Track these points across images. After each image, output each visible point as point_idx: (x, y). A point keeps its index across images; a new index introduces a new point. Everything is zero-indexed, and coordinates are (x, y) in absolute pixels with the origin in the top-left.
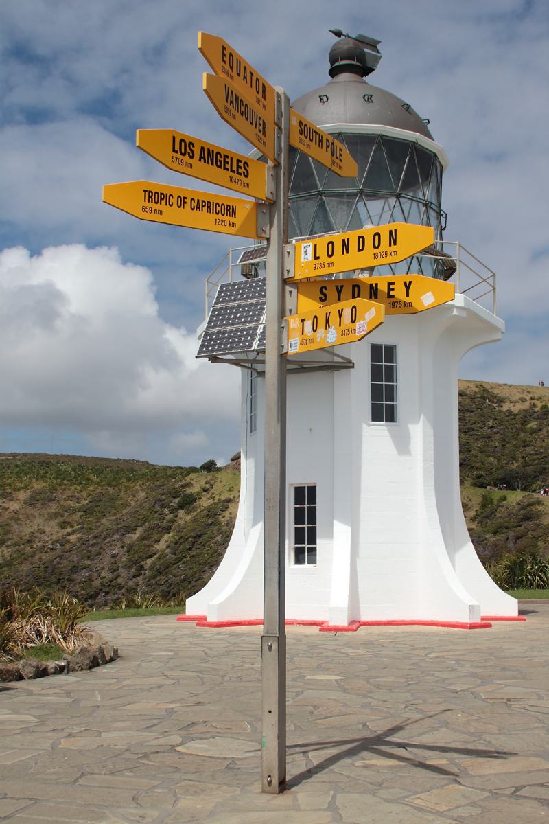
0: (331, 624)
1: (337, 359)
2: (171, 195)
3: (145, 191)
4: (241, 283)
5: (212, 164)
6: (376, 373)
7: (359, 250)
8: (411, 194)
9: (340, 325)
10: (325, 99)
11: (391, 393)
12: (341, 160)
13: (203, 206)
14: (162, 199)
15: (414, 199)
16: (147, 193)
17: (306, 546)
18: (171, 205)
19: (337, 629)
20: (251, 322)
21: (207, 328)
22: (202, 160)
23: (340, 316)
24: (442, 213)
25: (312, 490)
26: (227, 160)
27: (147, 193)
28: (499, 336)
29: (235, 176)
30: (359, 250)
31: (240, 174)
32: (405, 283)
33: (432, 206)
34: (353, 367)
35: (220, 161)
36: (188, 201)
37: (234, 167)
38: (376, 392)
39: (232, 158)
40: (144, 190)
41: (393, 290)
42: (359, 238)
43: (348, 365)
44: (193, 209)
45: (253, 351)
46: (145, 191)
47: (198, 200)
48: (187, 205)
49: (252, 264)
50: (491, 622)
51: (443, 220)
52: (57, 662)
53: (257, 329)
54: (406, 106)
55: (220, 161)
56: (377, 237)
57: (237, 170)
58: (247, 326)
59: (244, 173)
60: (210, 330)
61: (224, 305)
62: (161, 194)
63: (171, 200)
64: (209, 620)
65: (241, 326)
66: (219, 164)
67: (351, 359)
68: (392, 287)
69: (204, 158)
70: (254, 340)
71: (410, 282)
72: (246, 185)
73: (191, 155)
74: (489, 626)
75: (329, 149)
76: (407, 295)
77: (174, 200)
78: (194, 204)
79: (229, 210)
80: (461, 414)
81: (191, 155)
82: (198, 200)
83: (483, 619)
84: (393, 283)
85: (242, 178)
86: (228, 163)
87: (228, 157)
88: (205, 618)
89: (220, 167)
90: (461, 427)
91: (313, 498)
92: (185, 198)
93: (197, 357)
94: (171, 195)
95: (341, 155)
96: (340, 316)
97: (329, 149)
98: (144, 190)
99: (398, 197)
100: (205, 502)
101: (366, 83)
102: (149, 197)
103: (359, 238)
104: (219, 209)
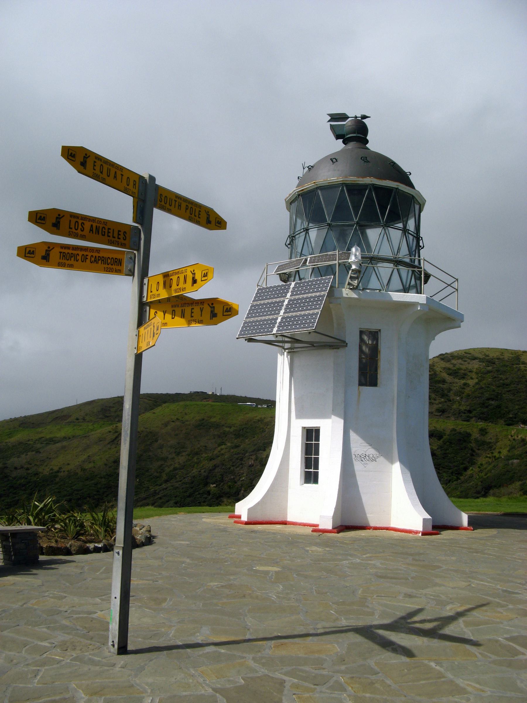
4: (279, 286)
5: (98, 234)
10: (334, 160)
12: (199, 218)
13: (98, 260)
14: (71, 257)
16: (62, 254)
23: (202, 311)
27: (62, 254)
44: (91, 263)
45: (274, 334)
47: (96, 257)
48: (88, 261)
51: (421, 241)
55: (104, 232)
61: (297, 297)
63: (78, 257)
66: (103, 233)
68: (193, 311)
75: (188, 211)
78: (93, 259)
82: (96, 257)
91: (317, 438)
93: (237, 338)
95: (199, 214)
96: (202, 311)
97: (188, 211)
102: (63, 256)
104: (109, 261)
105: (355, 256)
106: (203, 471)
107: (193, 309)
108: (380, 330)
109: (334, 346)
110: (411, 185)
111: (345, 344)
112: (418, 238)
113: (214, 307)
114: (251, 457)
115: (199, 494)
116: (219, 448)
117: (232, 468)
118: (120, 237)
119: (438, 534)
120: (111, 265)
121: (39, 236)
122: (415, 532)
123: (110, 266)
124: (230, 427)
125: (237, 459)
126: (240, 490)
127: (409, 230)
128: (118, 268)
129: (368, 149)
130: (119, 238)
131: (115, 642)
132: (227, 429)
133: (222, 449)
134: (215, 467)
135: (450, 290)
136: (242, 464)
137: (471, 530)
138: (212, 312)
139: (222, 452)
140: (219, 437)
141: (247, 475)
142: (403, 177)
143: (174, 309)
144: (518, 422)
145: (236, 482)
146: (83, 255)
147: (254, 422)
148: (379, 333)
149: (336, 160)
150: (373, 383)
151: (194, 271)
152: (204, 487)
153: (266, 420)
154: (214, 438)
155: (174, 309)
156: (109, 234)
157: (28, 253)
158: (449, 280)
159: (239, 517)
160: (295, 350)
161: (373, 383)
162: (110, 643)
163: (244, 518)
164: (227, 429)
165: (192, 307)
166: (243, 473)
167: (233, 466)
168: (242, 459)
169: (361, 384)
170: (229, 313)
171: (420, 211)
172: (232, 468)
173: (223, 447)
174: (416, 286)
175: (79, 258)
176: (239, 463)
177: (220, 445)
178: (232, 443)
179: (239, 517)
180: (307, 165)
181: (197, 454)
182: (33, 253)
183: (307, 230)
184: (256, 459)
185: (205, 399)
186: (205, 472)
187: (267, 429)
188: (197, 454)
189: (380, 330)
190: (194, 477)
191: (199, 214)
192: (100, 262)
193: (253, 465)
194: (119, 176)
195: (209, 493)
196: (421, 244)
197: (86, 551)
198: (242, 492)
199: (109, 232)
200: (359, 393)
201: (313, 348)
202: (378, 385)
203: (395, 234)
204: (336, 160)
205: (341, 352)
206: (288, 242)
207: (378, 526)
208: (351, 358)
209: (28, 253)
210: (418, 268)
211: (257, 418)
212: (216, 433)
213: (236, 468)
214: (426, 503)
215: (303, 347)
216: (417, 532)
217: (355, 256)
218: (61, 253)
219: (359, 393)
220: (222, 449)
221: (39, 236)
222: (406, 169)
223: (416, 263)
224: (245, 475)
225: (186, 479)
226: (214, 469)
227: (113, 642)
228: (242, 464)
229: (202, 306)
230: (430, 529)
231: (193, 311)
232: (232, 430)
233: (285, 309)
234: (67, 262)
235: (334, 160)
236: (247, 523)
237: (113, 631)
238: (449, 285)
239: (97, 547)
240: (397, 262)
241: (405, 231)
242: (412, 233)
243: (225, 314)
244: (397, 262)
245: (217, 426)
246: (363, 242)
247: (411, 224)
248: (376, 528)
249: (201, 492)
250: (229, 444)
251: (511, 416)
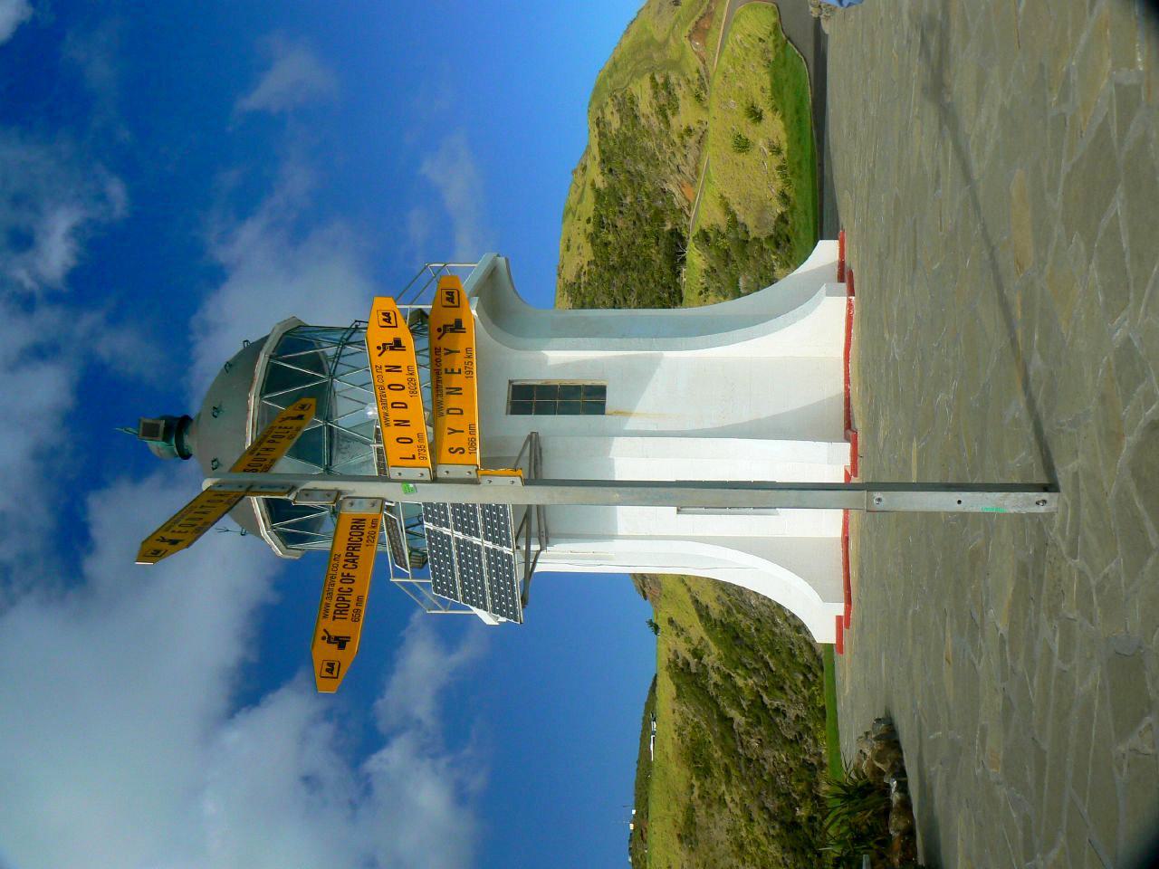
0: (848, 462)
1: (527, 453)
2: (339, 590)
7: (406, 407)
8: (330, 364)
9: (463, 432)
14: (344, 600)
15: (336, 360)
18: (351, 590)
19: (854, 455)
20: (479, 556)
21: (486, 609)
23: (455, 431)
24: (354, 327)
27: (337, 616)
28: (502, 260)
30: (406, 407)
33: (346, 337)
40: (334, 619)
41: (453, 370)
42: (393, 407)
43: (534, 441)
47: (346, 560)
48: (352, 572)
49: (410, 555)
50: (846, 271)
52: (893, 790)
53: (488, 548)
54: (228, 368)
56: (459, 411)
58: (484, 561)
60: (489, 605)
64: (842, 613)
65: (485, 568)
67: (526, 435)
68: (449, 371)
70: (502, 552)
74: (851, 274)
75: (277, 440)
78: (350, 565)
79: (358, 527)
80: (587, 306)
82: (346, 560)
88: (839, 619)
90: (633, 298)
96: (455, 431)
97: (277, 440)
98: (334, 619)
99: (332, 376)
100: (697, 630)
101: (199, 415)
102: (341, 614)
103: (393, 407)
104: (355, 539)
106: (772, 832)
107: (446, 370)
108: (510, 382)
109: (536, 460)
110: (265, 340)
111: (534, 435)
113: (445, 326)
114: (745, 744)
115: (813, 836)
116: (731, 805)
117: (765, 778)
119: (851, 272)
122: (849, 311)
123: (364, 537)
124: (692, 786)
125: (748, 768)
126: (804, 761)
131: (1037, 499)
132: (696, 792)
133: (733, 800)
134: (763, 808)
136: (758, 760)
137: (843, 232)
138: (452, 331)
139: (737, 799)
140: (709, 806)
141: (778, 750)
143: (445, 412)
144: (677, 284)
145: (791, 769)
146: (341, 581)
147: (682, 742)
148: (515, 383)
149: (215, 460)
150: (600, 391)
151: (379, 348)
152: (801, 827)
153: (679, 722)
154: (713, 815)
155: (445, 412)
160: (543, 529)
161: (600, 391)
162: (1042, 509)
164: (696, 792)
165: (443, 371)
166: (774, 757)
167: (762, 776)
168: (749, 760)
169: (603, 414)
170: (455, 295)
172: (765, 778)
173: (728, 798)
175: (345, 587)
176: (757, 766)
177: (725, 805)
178: (717, 696)
181: (741, 846)
182: (331, 665)
184: (748, 733)
185: (642, 835)
186: (774, 827)
187: (696, 720)
188: (741, 846)
189: (510, 382)
190: (783, 847)
191: (286, 428)
192: (355, 553)
193: (760, 740)
195: (811, 819)
197: (906, 805)
198: (807, 757)
200: (617, 413)
202: (604, 383)
204: (215, 460)
205: (547, 445)
207: (843, 378)
211: (676, 737)
212: (703, 812)
213: (765, 769)
214: (804, 296)
215: (539, 519)
216: (850, 305)
218: (334, 618)
219: (617, 413)
220: (733, 800)
224: (777, 753)
225: (789, 861)
226: (767, 808)
227: (1038, 503)
228: (758, 760)
229: (443, 352)
230: (844, 286)
231: (449, 371)
232: (697, 784)
233: (470, 535)
234: (353, 606)
235: (215, 463)
237: (1020, 504)
239: (897, 788)
243: (456, 304)
245: (690, 810)
248: (847, 380)
249: (810, 833)
250: (723, 788)
251: (666, 295)
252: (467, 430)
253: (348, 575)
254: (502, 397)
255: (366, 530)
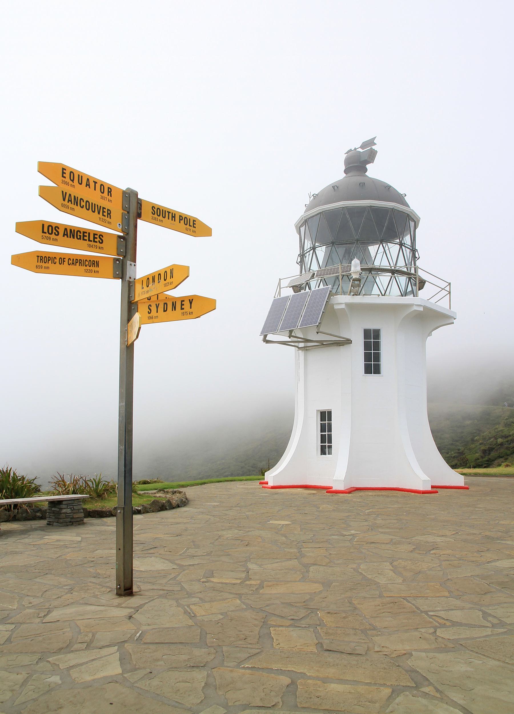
3: (38, 257)
6: (367, 346)
8: (398, 241)
11: (377, 357)
13: (76, 263)
14: (49, 260)
16: (39, 258)
17: (327, 444)
22: (66, 236)
25: (330, 413)
26: (85, 234)
27: (39, 258)
29: (92, 243)
31: (97, 242)
32: (190, 300)
34: (351, 343)
35: (80, 236)
36: (66, 260)
37: (95, 239)
38: (367, 357)
39: (89, 234)
43: (348, 342)
46: (38, 257)
47: (73, 259)
48: (66, 263)
50: (438, 490)
55: (80, 236)
57: (94, 240)
59: (99, 241)
62: (49, 257)
66: (79, 237)
68: (183, 303)
69: (67, 235)
71: (192, 300)
72: (102, 248)
73: (57, 233)
76: (191, 308)
77: (57, 261)
78: (70, 262)
81: (57, 233)
82: (73, 259)
83: (433, 487)
84: (184, 301)
85: (98, 244)
86: (86, 236)
87: (86, 233)
89: (80, 239)
91: (330, 419)
92: (64, 259)
94: (55, 258)
102: (41, 259)
105: (356, 266)
109: (339, 343)
110: (407, 205)
112: (414, 250)
118: (96, 240)
119: (437, 492)
120: (89, 267)
121: (32, 246)
123: (88, 267)
127: (404, 244)
128: (96, 269)
129: (367, 176)
130: (94, 241)
135: (444, 293)
142: (400, 199)
150: (377, 370)
156: (85, 238)
157: (19, 260)
158: (443, 285)
159: (267, 483)
161: (377, 370)
163: (271, 484)
171: (415, 228)
174: (412, 292)
179: (267, 483)
180: (312, 194)
183: (314, 249)
194: (92, 184)
196: (417, 256)
199: (84, 236)
201: (323, 346)
203: (393, 248)
206: (299, 260)
208: (357, 351)
209: (19, 260)
210: (414, 275)
217: (356, 266)
221: (32, 246)
222: (401, 191)
223: (413, 271)
236: (273, 488)
238: (443, 289)
240: (393, 272)
241: (401, 245)
242: (409, 247)
244: (393, 272)
246: (365, 258)
247: (407, 240)
252: (191, 310)
253: (64, 261)
254: (372, 326)
255: (93, 268)
